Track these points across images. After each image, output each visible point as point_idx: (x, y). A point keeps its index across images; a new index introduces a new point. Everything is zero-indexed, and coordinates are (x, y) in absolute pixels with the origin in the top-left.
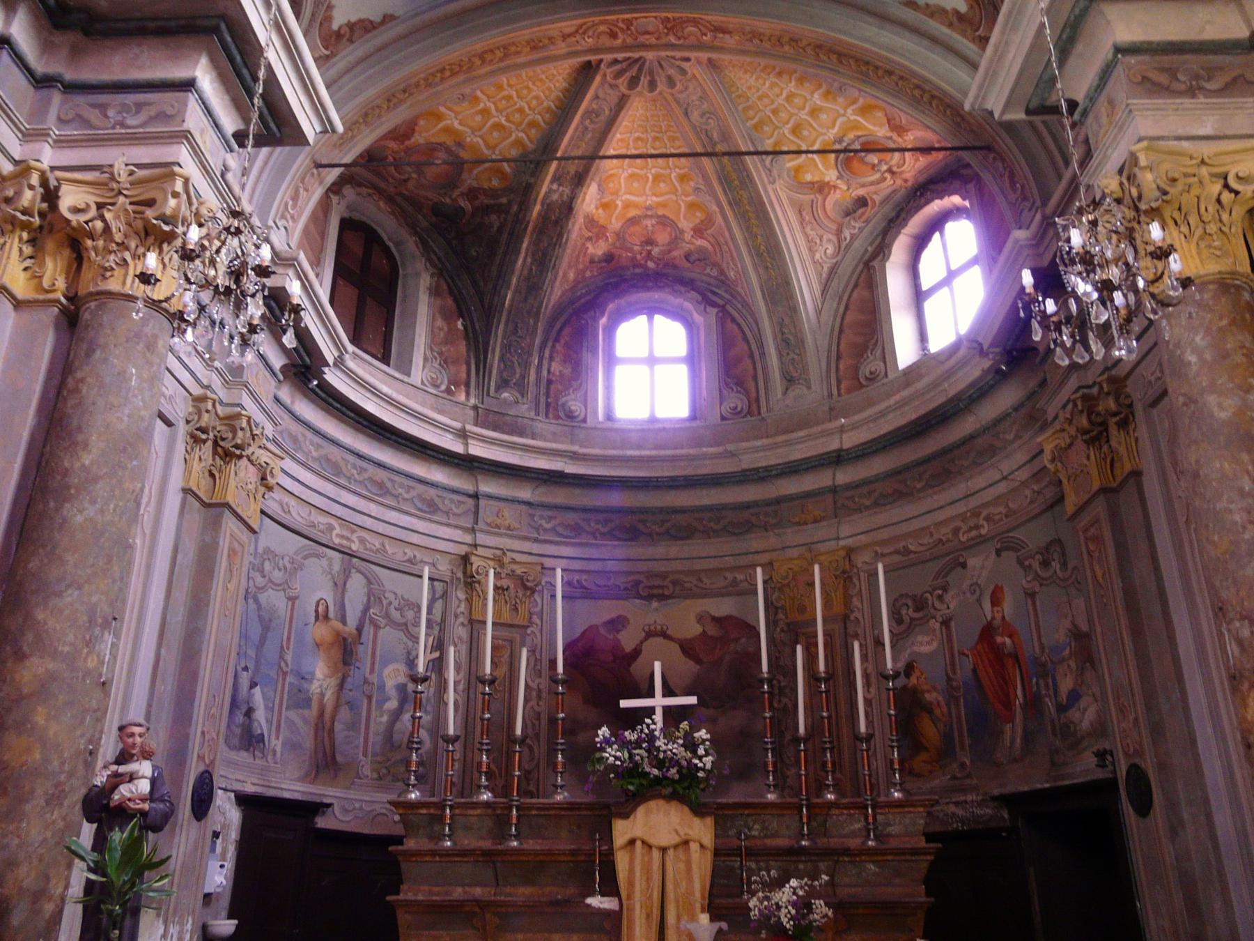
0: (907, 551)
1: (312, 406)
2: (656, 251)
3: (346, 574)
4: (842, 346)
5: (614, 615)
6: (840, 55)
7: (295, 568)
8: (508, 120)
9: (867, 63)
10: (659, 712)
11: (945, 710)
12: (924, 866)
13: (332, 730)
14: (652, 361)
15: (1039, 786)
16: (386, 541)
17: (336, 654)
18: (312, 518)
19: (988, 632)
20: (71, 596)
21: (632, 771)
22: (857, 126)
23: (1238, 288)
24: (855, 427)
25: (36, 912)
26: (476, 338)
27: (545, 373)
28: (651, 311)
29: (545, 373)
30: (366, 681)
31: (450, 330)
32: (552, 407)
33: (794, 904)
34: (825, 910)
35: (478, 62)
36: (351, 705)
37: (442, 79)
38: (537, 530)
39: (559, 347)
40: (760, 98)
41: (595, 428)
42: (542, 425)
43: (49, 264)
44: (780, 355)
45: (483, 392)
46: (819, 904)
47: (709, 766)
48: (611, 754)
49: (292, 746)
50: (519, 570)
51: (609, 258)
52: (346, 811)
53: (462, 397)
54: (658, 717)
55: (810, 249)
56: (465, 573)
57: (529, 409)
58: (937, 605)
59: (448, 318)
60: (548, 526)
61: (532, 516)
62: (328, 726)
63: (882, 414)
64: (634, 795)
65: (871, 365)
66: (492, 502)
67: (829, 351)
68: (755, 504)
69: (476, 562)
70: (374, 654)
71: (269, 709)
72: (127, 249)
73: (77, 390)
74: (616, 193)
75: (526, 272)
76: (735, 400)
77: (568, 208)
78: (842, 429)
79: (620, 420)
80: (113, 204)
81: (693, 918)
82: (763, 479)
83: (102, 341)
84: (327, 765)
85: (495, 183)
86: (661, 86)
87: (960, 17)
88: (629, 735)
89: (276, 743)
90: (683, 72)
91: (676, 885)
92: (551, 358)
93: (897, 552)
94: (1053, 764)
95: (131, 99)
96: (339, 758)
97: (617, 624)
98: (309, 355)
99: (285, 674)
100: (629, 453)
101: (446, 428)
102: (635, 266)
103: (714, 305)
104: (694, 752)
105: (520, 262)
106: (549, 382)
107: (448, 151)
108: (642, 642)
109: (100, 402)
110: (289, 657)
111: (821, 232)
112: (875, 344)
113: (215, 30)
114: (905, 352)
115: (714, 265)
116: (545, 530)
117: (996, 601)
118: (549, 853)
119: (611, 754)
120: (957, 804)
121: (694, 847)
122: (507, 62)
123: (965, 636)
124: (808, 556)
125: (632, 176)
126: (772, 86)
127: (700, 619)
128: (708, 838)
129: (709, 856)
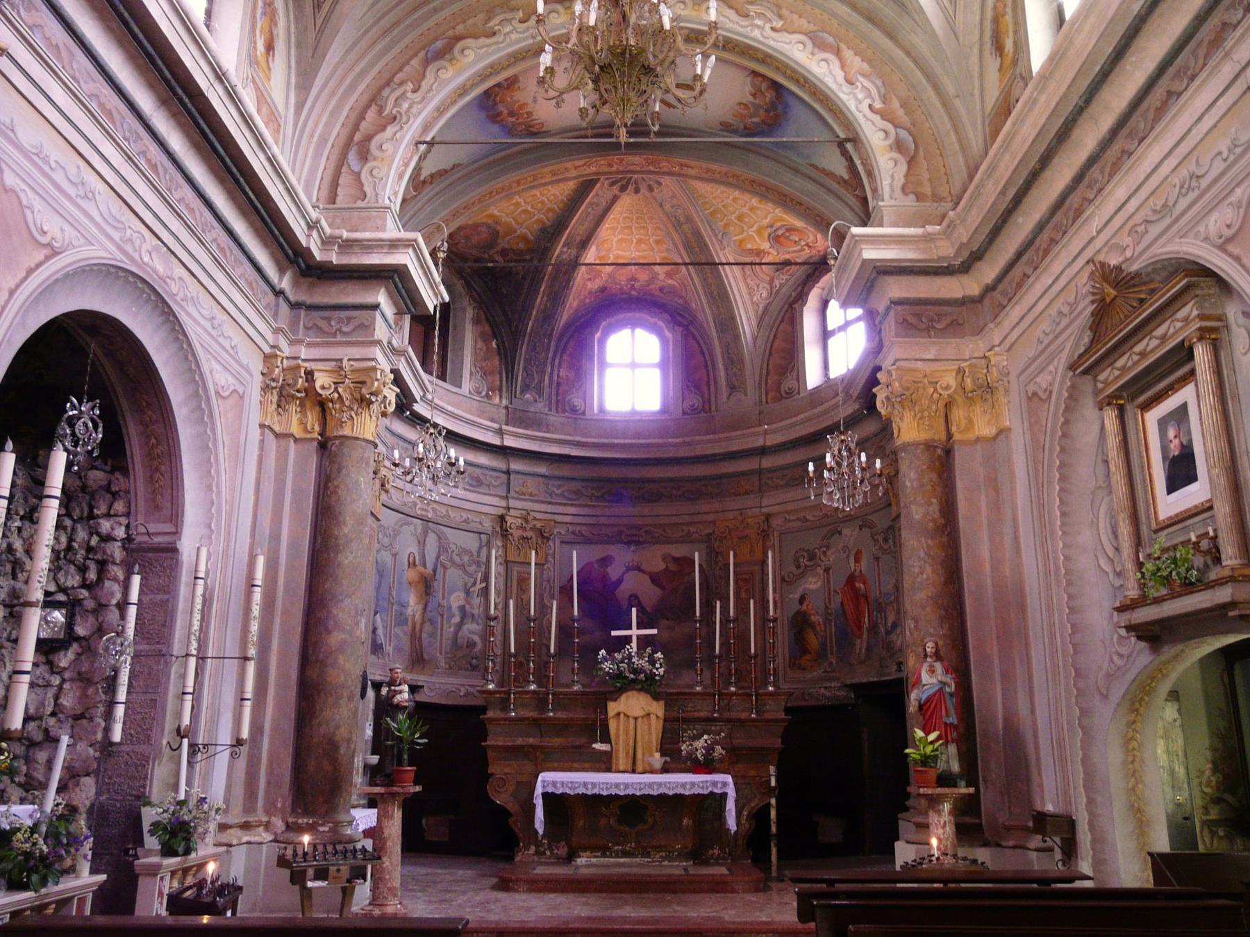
0: (805, 520)
1: (403, 423)
2: (637, 285)
3: (425, 534)
4: (770, 367)
5: (604, 555)
6: (768, 189)
7: (396, 533)
8: (532, 207)
9: (785, 196)
10: (634, 639)
11: (823, 628)
12: (781, 730)
13: (420, 638)
14: (633, 365)
15: (871, 679)
16: (450, 509)
17: (421, 587)
18: (404, 499)
19: (851, 579)
20: (347, 601)
21: (619, 676)
22: (782, 219)
23: (936, 447)
24: (774, 432)
25: (349, 747)
26: (506, 357)
27: (555, 378)
28: (634, 325)
29: (555, 378)
30: (440, 605)
31: (487, 349)
32: (561, 404)
33: (704, 748)
34: (721, 751)
35: (515, 185)
36: (432, 622)
37: (490, 198)
38: (550, 494)
39: (565, 357)
40: (714, 198)
41: (592, 419)
42: (555, 419)
43: (309, 415)
44: (726, 369)
45: (512, 394)
46: (718, 748)
47: (662, 673)
48: (607, 666)
49: (398, 649)
50: (539, 525)
51: (603, 290)
52: (431, 690)
53: (497, 400)
54: (634, 644)
55: (750, 294)
56: (501, 528)
57: (545, 406)
58: (823, 558)
59: (486, 341)
60: (558, 492)
61: (547, 485)
62: (418, 636)
63: (793, 425)
64: (620, 689)
65: (789, 383)
66: (520, 477)
67: (761, 369)
68: (705, 478)
69: (509, 520)
70: (444, 587)
71: (385, 627)
72: (352, 409)
73: (336, 492)
74: (609, 250)
75: (542, 307)
76: (695, 400)
77: (575, 264)
78: (766, 433)
79: (609, 413)
80: (343, 383)
81: (651, 755)
82: (709, 461)
83: (345, 464)
84: (418, 661)
85: (521, 246)
86: (643, 190)
87: (845, 182)
88: (618, 656)
89: (389, 649)
90: (660, 184)
91: (643, 737)
92: (560, 365)
93: (798, 519)
94: (881, 666)
95: (344, 314)
96: (426, 656)
97: (605, 561)
98: (405, 397)
99: (392, 604)
100: (616, 441)
101: (488, 429)
102: (622, 294)
103: (680, 324)
104: (654, 665)
105: (538, 300)
106: (559, 384)
107: (489, 227)
108: (623, 574)
109: (348, 499)
110: (394, 593)
111: (758, 282)
112: (793, 367)
113: (392, 278)
114: (813, 378)
115: (681, 297)
116: (556, 495)
117: (857, 560)
118: (572, 719)
119: (607, 666)
120: (826, 688)
121: (653, 717)
122: (536, 183)
123: (839, 580)
124: (740, 518)
125: (621, 240)
126: (722, 192)
127: (664, 559)
128: (661, 713)
129: (661, 722)
